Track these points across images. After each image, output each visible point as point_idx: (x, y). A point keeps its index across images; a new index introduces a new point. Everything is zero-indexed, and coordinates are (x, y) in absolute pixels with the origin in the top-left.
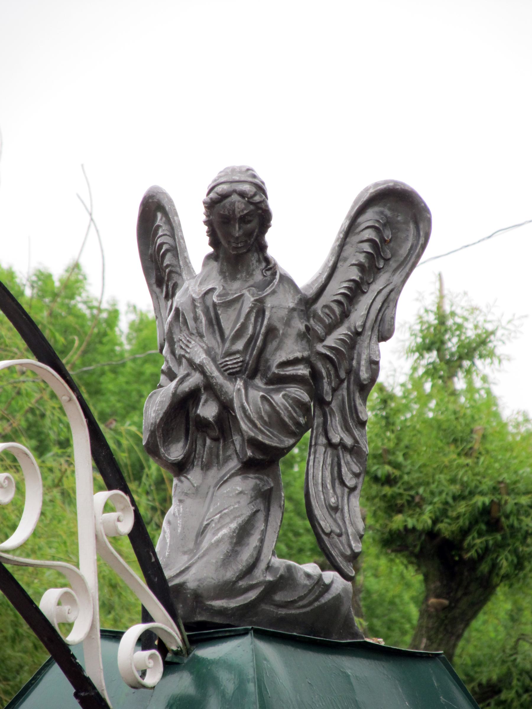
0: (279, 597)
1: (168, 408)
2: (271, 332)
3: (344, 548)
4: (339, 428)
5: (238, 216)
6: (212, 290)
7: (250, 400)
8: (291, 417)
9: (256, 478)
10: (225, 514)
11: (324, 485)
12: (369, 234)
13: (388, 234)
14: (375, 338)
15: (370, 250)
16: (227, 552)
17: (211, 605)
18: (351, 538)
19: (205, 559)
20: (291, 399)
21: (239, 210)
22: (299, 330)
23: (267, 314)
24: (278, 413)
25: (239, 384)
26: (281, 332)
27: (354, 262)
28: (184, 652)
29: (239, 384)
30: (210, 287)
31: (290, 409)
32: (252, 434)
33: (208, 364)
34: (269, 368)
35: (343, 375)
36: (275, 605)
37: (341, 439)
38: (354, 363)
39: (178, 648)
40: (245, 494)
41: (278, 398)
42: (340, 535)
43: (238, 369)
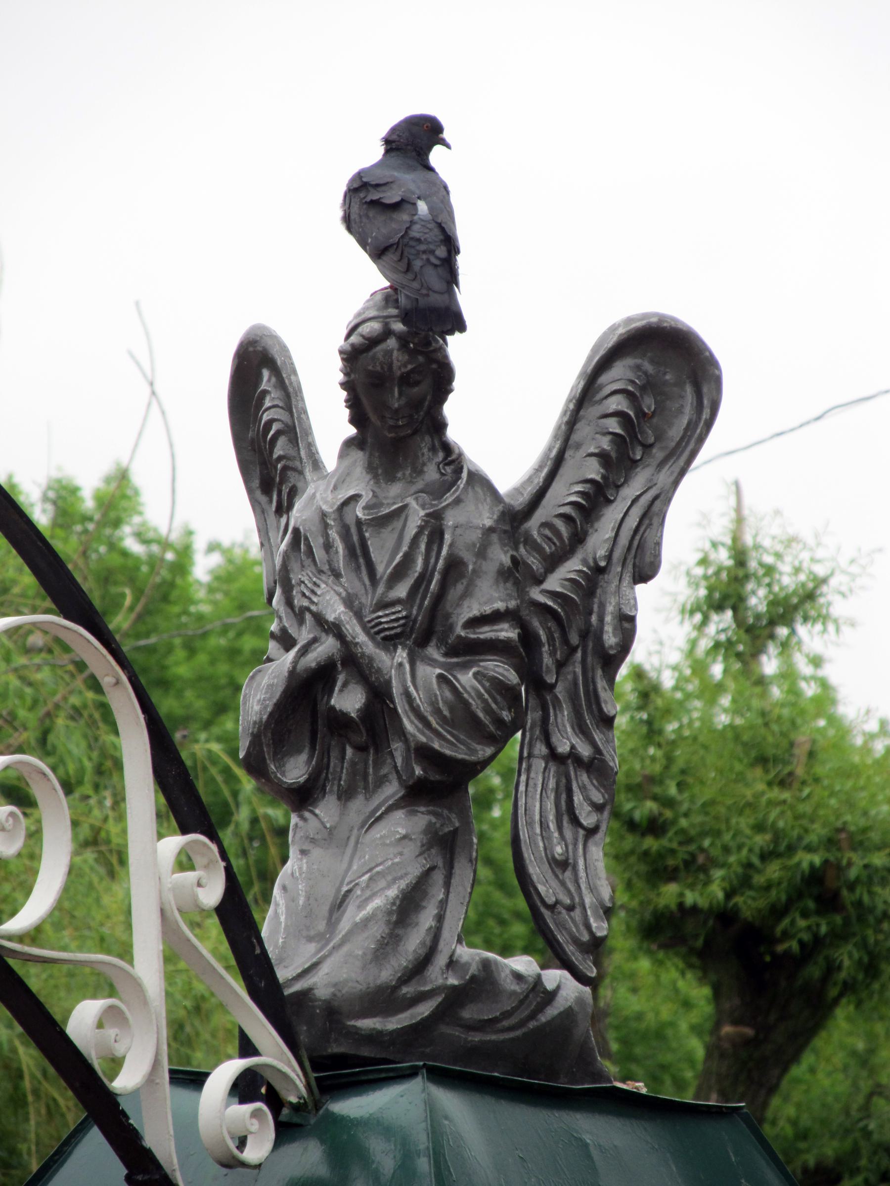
0: (468, 1013)
1: (281, 696)
2: (454, 566)
3: (578, 930)
4: (569, 729)
5: (398, 373)
6: (355, 498)
7: (420, 682)
8: (488, 710)
9: (429, 813)
10: (378, 873)
11: (543, 825)
12: (616, 403)
13: (649, 404)
14: (627, 578)
15: (619, 431)
16: (382, 937)
17: (355, 1026)
18: (589, 913)
19: (345, 949)
20: (488, 681)
21: (399, 364)
22: (502, 564)
23: (448, 537)
24: (466, 704)
25: (401, 655)
26: (471, 567)
27: (592, 450)
28: (310, 1106)
29: (401, 655)
30: (351, 492)
31: (486, 696)
32: (423, 739)
33: (348, 623)
34: (451, 628)
35: (574, 639)
36: (461, 1026)
37: (573, 747)
38: (594, 619)
39: (300, 1098)
40: (411, 839)
41: (466, 679)
42: (571, 908)
43: (399, 630)
